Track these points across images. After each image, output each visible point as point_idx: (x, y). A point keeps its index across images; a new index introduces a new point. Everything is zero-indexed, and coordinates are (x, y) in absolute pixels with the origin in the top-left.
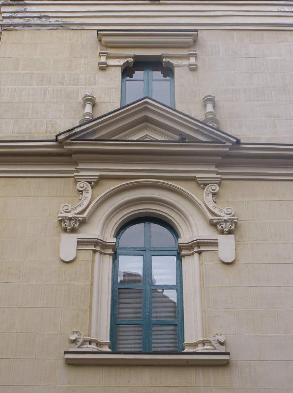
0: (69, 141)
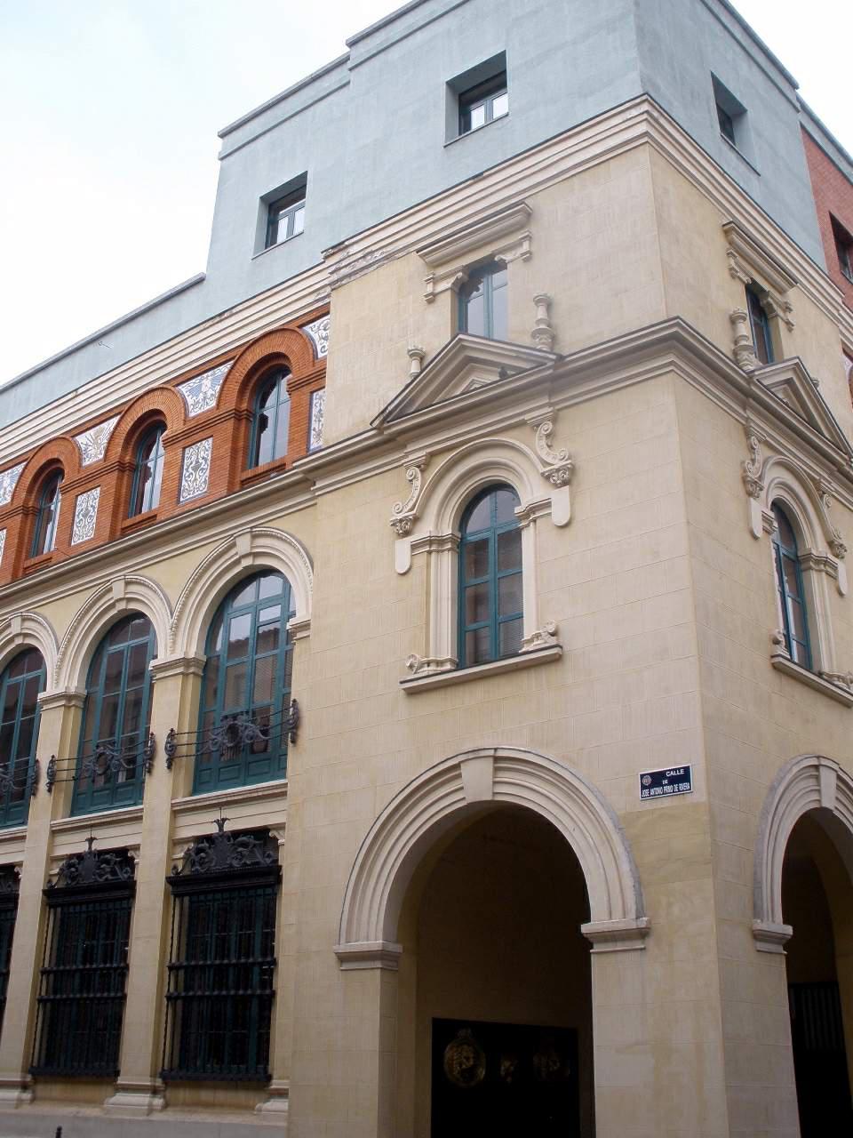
0: (386, 425)
